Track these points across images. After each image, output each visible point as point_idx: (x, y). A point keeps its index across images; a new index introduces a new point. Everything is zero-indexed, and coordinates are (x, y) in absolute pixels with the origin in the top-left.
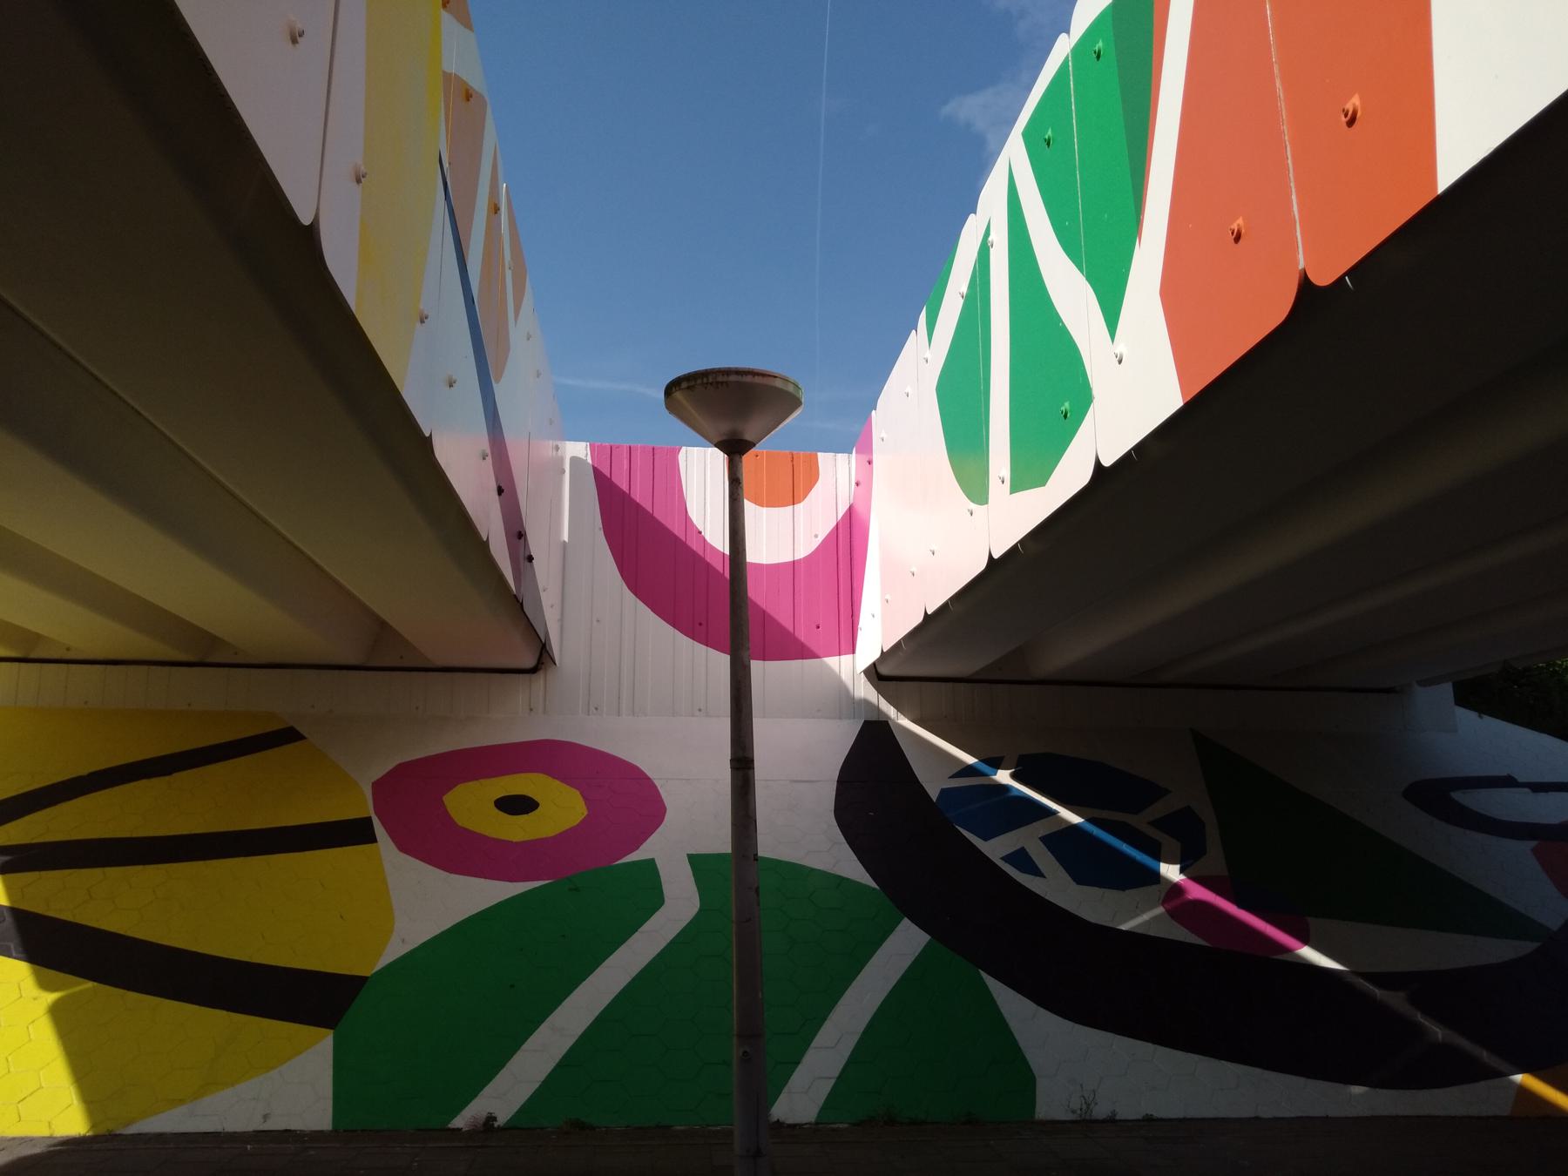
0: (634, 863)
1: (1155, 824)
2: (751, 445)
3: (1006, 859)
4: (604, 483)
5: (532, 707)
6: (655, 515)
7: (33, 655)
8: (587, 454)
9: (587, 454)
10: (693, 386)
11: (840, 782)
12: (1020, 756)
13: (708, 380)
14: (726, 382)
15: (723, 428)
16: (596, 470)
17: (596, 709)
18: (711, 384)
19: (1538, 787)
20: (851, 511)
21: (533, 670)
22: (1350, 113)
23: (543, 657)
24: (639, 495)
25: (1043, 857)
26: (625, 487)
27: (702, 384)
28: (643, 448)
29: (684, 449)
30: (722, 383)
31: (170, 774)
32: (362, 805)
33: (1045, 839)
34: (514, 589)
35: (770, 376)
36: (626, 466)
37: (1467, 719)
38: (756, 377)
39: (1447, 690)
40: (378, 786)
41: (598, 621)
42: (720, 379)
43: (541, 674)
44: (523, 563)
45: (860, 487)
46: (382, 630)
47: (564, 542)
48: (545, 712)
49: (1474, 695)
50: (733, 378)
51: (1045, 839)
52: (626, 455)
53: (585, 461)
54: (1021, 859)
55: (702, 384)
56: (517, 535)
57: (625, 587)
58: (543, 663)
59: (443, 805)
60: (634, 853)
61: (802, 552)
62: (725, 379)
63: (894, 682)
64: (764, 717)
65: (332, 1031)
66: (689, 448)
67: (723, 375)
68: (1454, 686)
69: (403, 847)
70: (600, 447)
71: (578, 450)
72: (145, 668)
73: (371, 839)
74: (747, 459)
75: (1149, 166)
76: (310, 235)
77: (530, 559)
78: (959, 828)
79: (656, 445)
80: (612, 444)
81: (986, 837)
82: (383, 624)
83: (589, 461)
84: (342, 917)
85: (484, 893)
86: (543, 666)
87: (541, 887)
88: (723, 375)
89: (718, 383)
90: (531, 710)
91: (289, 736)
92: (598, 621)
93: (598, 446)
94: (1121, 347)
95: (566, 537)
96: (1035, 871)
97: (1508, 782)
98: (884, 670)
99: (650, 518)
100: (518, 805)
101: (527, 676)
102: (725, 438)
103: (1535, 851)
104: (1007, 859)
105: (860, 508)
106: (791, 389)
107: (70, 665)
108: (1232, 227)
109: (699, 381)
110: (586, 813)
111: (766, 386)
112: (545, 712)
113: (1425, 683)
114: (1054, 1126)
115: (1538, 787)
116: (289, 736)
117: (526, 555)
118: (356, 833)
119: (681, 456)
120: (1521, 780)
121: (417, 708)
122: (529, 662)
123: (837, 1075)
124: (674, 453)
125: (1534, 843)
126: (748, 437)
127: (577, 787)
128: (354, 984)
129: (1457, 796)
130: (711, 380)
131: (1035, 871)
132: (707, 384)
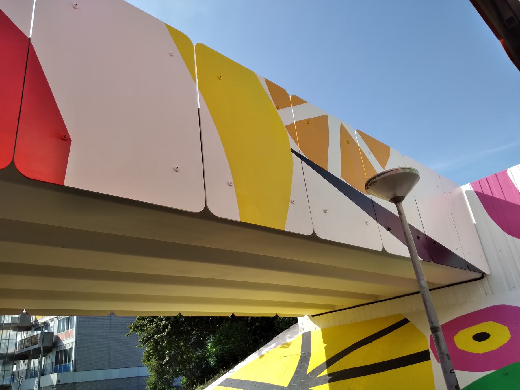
4: (481, 196)
5: (487, 293)
6: (507, 200)
7: (335, 310)
8: (471, 188)
9: (471, 188)
10: (368, 187)
16: (477, 193)
17: (514, 287)
18: (372, 184)
24: (497, 195)
26: (490, 194)
27: (369, 185)
28: (492, 176)
29: (508, 169)
30: (374, 182)
31: (371, 342)
36: (487, 186)
38: (385, 174)
41: (500, 251)
42: (373, 181)
47: (474, 224)
48: (492, 293)
52: (485, 181)
53: (471, 190)
55: (369, 185)
57: (505, 233)
60: (313, 388)
66: (510, 168)
70: (475, 183)
71: (467, 187)
73: (429, 358)
79: (496, 173)
80: (479, 180)
83: (473, 190)
87: (491, 373)
89: (373, 183)
90: (487, 294)
91: (405, 321)
92: (500, 251)
93: (474, 183)
95: (474, 222)
99: (505, 202)
100: (481, 337)
101: (480, 280)
109: (368, 185)
112: (492, 293)
116: (405, 321)
119: (509, 173)
121: (445, 302)
124: (505, 173)
127: (507, 326)
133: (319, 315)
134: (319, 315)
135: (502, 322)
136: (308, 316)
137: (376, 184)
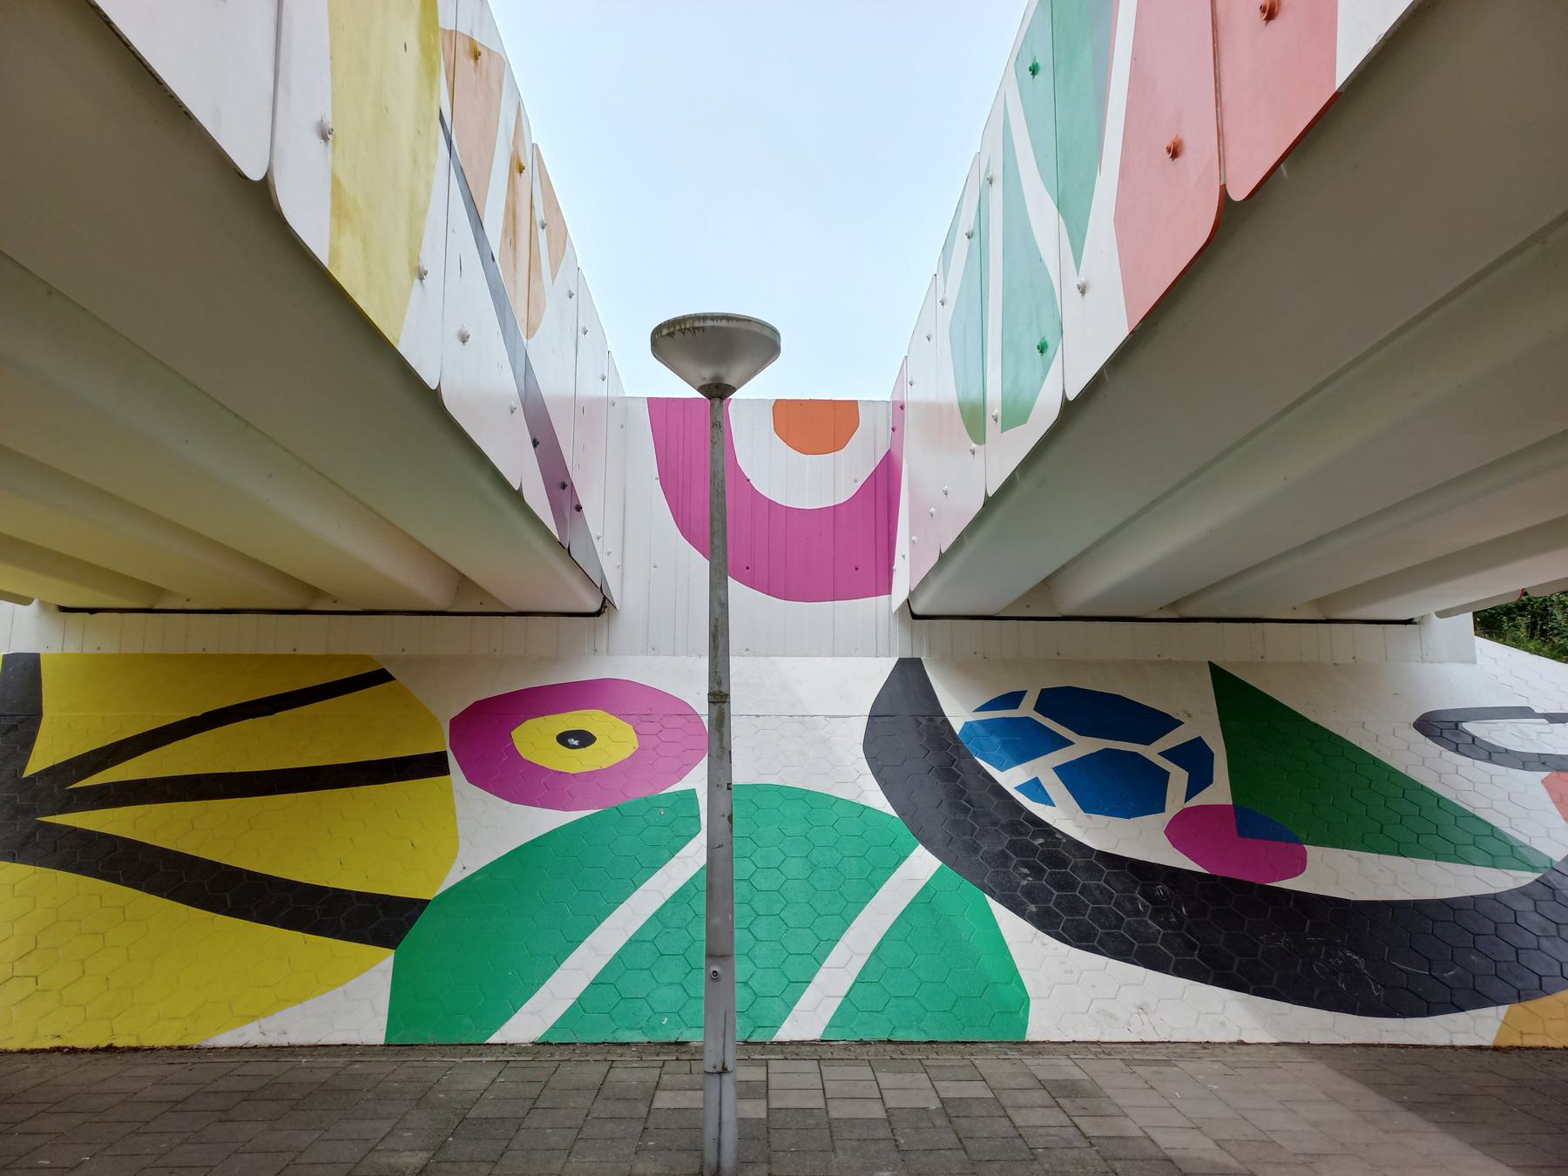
0: (676, 793)
1: (1166, 754)
2: (733, 390)
3: (1020, 788)
11: (873, 716)
12: (1042, 690)
13: (685, 326)
15: (707, 374)
18: (689, 329)
21: (598, 614)
23: (605, 606)
25: (1055, 787)
27: (680, 330)
30: (698, 328)
32: (441, 742)
33: (1058, 770)
34: (558, 537)
39: (1467, 619)
40: (456, 723)
42: (697, 324)
43: (604, 616)
44: (568, 511)
45: (896, 432)
46: (463, 582)
49: (1491, 623)
50: (709, 323)
51: (1058, 770)
54: (1035, 789)
56: (560, 486)
58: (606, 607)
59: (510, 739)
61: (842, 498)
62: (702, 324)
64: (833, 656)
65: (392, 952)
67: (699, 321)
68: (1475, 614)
69: (474, 777)
76: (262, 194)
77: (579, 508)
78: (978, 759)
82: (463, 576)
84: (412, 845)
85: (546, 820)
86: (606, 610)
88: (699, 321)
89: (694, 328)
97: (1525, 712)
98: (918, 608)
105: (895, 452)
110: (637, 746)
111: (749, 331)
114: (1040, 1048)
117: (575, 505)
118: (433, 765)
120: (1538, 711)
122: (594, 606)
123: (844, 994)
125: (1545, 774)
126: (729, 381)
128: (413, 907)
129: (1470, 727)
130: (688, 326)
131: (1046, 800)
132: (685, 329)
133: (92, 611)
134: (92, 611)
135: (622, 716)
136: (44, 605)
137: (699, 334)
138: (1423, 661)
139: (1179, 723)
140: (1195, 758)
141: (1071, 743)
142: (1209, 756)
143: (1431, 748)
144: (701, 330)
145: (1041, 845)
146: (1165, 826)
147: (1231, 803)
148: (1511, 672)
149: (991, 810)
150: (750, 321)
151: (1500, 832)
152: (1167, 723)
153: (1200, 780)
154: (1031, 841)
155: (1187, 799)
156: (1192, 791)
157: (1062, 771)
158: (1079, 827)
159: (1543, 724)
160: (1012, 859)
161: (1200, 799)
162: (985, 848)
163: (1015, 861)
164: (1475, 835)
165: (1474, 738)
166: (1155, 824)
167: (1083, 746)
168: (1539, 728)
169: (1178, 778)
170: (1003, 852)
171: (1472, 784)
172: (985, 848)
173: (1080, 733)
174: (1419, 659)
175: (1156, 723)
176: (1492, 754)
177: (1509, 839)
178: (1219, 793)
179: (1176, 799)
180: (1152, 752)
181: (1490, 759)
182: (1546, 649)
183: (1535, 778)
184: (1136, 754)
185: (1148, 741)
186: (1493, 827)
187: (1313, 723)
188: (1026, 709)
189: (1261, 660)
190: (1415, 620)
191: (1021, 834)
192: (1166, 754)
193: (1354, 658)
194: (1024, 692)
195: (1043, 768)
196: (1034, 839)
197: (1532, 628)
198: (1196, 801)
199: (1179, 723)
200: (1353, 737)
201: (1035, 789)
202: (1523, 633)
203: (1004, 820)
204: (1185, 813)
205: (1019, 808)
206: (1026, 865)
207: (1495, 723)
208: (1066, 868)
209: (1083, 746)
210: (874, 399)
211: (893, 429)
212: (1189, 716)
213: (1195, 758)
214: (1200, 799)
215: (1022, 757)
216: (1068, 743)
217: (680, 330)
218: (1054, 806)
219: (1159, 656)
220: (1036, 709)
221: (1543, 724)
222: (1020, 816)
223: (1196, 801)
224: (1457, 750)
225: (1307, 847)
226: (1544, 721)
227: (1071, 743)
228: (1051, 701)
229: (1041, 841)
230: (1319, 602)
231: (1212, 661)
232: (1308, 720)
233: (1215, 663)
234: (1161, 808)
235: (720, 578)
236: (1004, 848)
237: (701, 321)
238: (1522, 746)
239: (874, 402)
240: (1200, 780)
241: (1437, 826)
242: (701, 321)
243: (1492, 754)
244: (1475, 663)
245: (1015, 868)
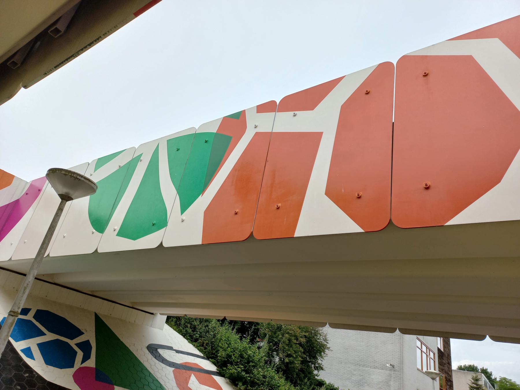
1: (77, 345)
10: (67, 175)
14: (80, 179)
15: (64, 191)
18: (74, 177)
19: (178, 352)
20: (17, 202)
22: (278, 207)
25: (36, 352)
27: (71, 176)
30: (78, 179)
35: (94, 183)
37: (167, 327)
38: (90, 182)
39: (165, 317)
42: (78, 177)
49: (169, 320)
50: (82, 179)
54: (28, 352)
62: (80, 178)
63: (43, 282)
68: (168, 316)
72: (60, 287)
74: (68, 203)
75: (46, 74)
81: (17, 340)
89: (76, 178)
94: (184, 217)
96: (31, 356)
97: (171, 348)
102: (63, 194)
103: (173, 371)
104: (23, 351)
106: (95, 188)
107: (146, 313)
108: (236, 211)
110: (189, 385)
113: (161, 314)
115: (178, 352)
120: (174, 349)
125: (173, 369)
126: (73, 197)
129: (160, 351)
130: (74, 176)
131: (31, 356)
132: (72, 176)
138: (151, 326)
139: (83, 333)
140: (85, 347)
141: (45, 334)
142: (91, 348)
143: (150, 356)
144: (79, 179)
145: (27, 376)
146: (73, 373)
147: (95, 367)
148: (169, 335)
149: (9, 359)
150: (95, 184)
151: (163, 387)
152: (79, 333)
153: (86, 357)
154: (23, 374)
155: (81, 364)
156: (84, 361)
157: (40, 346)
158: (43, 370)
159: (174, 353)
160: (14, 382)
161: (85, 365)
162: (4, 376)
163: (15, 383)
164: (157, 387)
165: (160, 354)
166: (71, 371)
167: (49, 337)
168: (173, 353)
169: (80, 355)
170: (11, 378)
171: (158, 370)
172: (4, 376)
173: (49, 331)
174: (150, 326)
175: (75, 332)
176: (164, 361)
177: (164, 389)
178: (91, 363)
179: (78, 364)
180: (73, 343)
181: (163, 362)
182: (177, 329)
183: (171, 369)
184: (67, 343)
185: (72, 339)
186: (161, 385)
187: (121, 341)
188: (30, 317)
189: (110, 315)
190: (154, 314)
191: (20, 371)
192: (77, 345)
193: (135, 321)
194: (31, 309)
195: (33, 343)
196: (25, 374)
197: (176, 322)
198: (84, 365)
199: (83, 333)
200: (132, 349)
201: (28, 352)
202: (173, 323)
203: (13, 364)
204: (80, 369)
205: (20, 359)
206: (19, 385)
207: (165, 350)
208: (35, 388)
209: (49, 337)
210: (22, 179)
211: (27, 194)
212: (86, 331)
213: (85, 347)
214: (85, 365)
215: (26, 336)
216: (44, 334)
217: (71, 176)
218: (34, 359)
219: (111, 315)
220: (34, 317)
221: (174, 353)
222: (20, 363)
223: (84, 365)
224: (156, 358)
225: (115, 387)
226: (175, 352)
227: (45, 334)
228: (40, 315)
229: (27, 375)
230: (132, 303)
231: (96, 312)
232: (120, 340)
233: (97, 313)
234: (72, 366)
235: (38, 266)
236: (12, 376)
237: (80, 177)
238: (169, 359)
239: (21, 180)
240: (86, 357)
241: (149, 382)
242: (80, 177)
243: (164, 361)
244: (163, 330)
245: (15, 386)
